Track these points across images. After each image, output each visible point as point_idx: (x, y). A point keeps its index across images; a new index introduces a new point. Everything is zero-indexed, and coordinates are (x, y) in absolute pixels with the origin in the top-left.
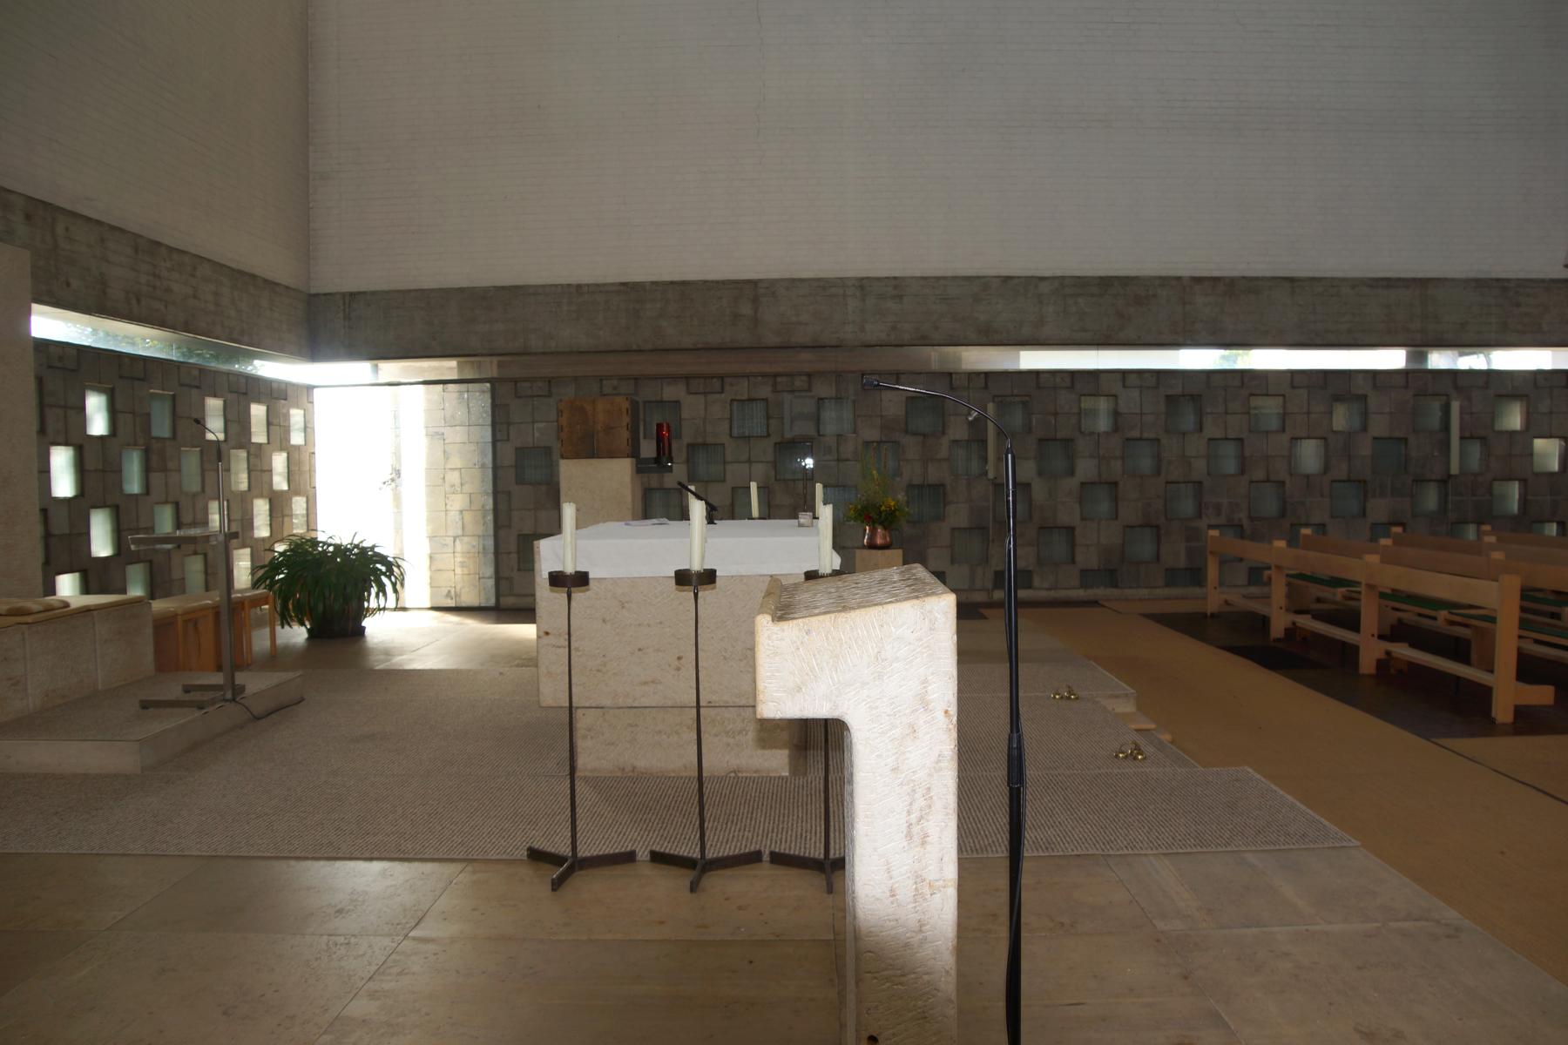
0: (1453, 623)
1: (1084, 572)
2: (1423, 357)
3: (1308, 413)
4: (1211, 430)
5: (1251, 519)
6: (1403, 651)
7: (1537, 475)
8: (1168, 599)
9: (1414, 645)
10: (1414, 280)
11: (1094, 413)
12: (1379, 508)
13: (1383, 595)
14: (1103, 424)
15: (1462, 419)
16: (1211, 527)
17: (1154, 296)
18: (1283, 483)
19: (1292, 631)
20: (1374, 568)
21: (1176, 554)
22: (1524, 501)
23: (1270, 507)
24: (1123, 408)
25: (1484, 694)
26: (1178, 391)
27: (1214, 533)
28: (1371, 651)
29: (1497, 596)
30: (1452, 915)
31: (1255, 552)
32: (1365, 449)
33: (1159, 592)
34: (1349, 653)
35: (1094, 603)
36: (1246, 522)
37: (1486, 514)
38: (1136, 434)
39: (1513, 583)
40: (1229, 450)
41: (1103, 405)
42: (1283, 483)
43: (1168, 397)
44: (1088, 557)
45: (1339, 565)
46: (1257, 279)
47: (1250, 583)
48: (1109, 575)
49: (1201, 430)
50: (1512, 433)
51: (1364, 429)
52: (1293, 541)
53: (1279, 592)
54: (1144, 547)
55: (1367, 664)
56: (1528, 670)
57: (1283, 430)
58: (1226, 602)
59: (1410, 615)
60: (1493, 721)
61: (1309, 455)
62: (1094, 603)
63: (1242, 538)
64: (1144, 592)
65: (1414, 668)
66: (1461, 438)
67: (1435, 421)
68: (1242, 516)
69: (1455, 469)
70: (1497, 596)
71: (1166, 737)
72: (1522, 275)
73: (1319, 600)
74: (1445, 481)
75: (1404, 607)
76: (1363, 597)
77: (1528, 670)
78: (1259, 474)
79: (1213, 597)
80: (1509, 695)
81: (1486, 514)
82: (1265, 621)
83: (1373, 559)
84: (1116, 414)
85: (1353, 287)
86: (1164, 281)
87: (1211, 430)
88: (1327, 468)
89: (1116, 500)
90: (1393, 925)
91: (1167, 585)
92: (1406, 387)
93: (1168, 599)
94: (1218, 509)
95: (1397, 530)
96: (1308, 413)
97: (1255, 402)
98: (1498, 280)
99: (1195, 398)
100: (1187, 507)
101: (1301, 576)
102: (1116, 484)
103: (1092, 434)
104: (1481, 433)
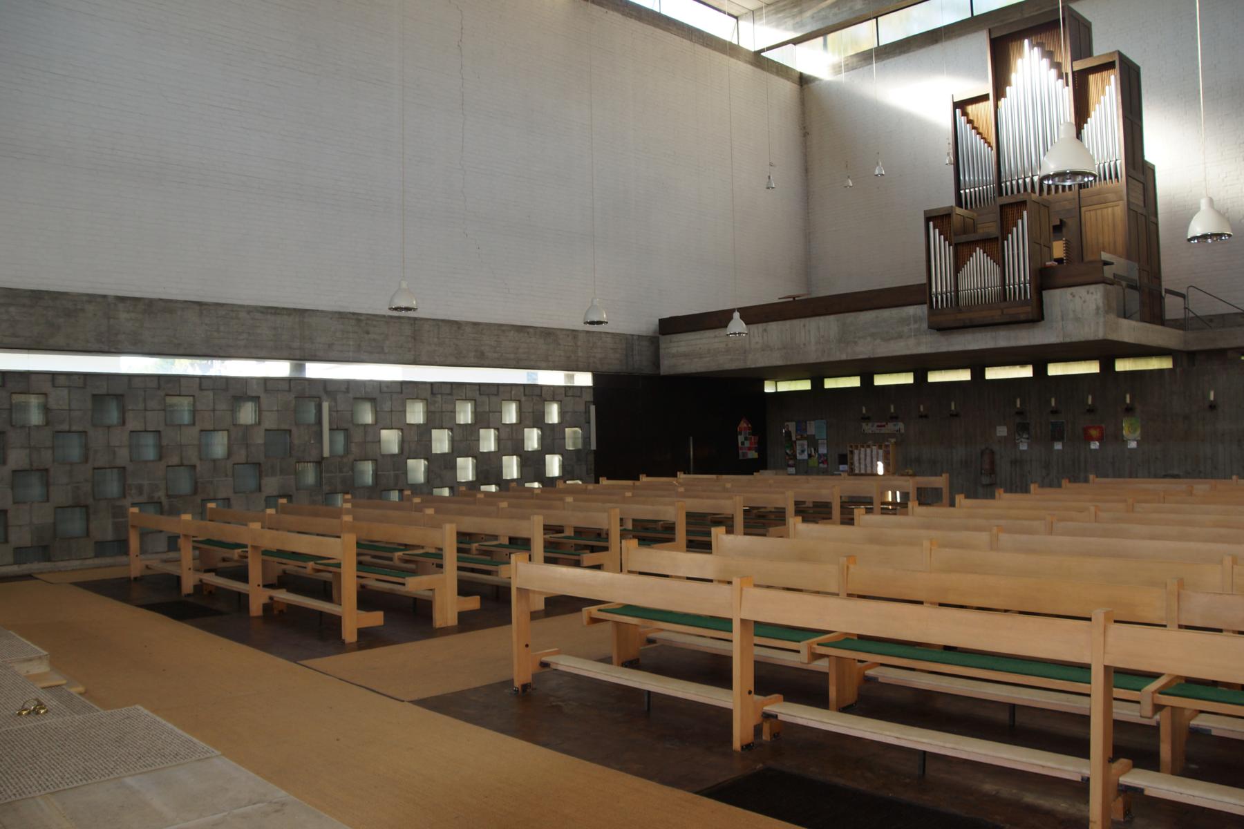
0: (319, 571)
1: (18, 550)
2: (301, 368)
3: (214, 410)
4: (133, 424)
5: (168, 496)
6: (283, 596)
7: (383, 456)
8: (100, 567)
9: (290, 590)
10: (295, 310)
11: (25, 407)
12: (272, 484)
13: (266, 553)
14: (35, 418)
15: (330, 415)
16: (134, 505)
17: (83, 310)
18: (194, 467)
19: (200, 587)
20: (256, 533)
21: (104, 528)
22: (376, 475)
23: (184, 486)
24: (52, 404)
25: (334, 623)
26: (103, 391)
27: (135, 510)
28: (258, 598)
29: (341, 549)
30: (281, 794)
31: (169, 525)
32: (259, 439)
33: (89, 562)
34: (241, 600)
35: (29, 577)
36: (164, 500)
37: (350, 486)
38: (65, 427)
39: (350, 539)
40: (149, 440)
41: (34, 401)
42: (194, 467)
43: (94, 396)
44: (21, 536)
45: (230, 532)
46: (171, 301)
47: (169, 550)
48: (44, 549)
49: (124, 423)
50: (366, 426)
51: (259, 423)
52: (202, 514)
53: (187, 555)
54: (75, 525)
55: (256, 608)
56: (367, 600)
57: (194, 424)
58: (147, 567)
59: (291, 566)
60: (343, 642)
61: (219, 445)
62: (29, 577)
63: (162, 513)
64: (76, 564)
65: (292, 607)
66: (331, 430)
67: (311, 417)
68: (161, 494)
69: (326, 453)
70: (341, 549)
71: (76, 690)
72: (370, 312)
73: (224, 560)
74: (319, 462)
75: (284, 561)
76: (249, 554)
77: (367, 600)
78: (175, 460)
79: (136, 564)
80: (353, 619)
81: (350, 486)
82: (178, 579)
83: (256, 526)
84: (46, 409)
85: (249, 312)
86: (92, 298)
87: (133, 424)
88: (230, 454)
89: (47, 485)
90: (236, 811)
91: (96, 556)
92: (290, 390)
93: (100, 567)
94: (140, 489)
95: (284, 501)
96: (214, 410)
97: (169, 400)
98: (354, 314)
99: (119, 397)
100: (113, 488)
101: (209, 542)
102: (47, 470)
103: (23, 427)
104: (346, 426)
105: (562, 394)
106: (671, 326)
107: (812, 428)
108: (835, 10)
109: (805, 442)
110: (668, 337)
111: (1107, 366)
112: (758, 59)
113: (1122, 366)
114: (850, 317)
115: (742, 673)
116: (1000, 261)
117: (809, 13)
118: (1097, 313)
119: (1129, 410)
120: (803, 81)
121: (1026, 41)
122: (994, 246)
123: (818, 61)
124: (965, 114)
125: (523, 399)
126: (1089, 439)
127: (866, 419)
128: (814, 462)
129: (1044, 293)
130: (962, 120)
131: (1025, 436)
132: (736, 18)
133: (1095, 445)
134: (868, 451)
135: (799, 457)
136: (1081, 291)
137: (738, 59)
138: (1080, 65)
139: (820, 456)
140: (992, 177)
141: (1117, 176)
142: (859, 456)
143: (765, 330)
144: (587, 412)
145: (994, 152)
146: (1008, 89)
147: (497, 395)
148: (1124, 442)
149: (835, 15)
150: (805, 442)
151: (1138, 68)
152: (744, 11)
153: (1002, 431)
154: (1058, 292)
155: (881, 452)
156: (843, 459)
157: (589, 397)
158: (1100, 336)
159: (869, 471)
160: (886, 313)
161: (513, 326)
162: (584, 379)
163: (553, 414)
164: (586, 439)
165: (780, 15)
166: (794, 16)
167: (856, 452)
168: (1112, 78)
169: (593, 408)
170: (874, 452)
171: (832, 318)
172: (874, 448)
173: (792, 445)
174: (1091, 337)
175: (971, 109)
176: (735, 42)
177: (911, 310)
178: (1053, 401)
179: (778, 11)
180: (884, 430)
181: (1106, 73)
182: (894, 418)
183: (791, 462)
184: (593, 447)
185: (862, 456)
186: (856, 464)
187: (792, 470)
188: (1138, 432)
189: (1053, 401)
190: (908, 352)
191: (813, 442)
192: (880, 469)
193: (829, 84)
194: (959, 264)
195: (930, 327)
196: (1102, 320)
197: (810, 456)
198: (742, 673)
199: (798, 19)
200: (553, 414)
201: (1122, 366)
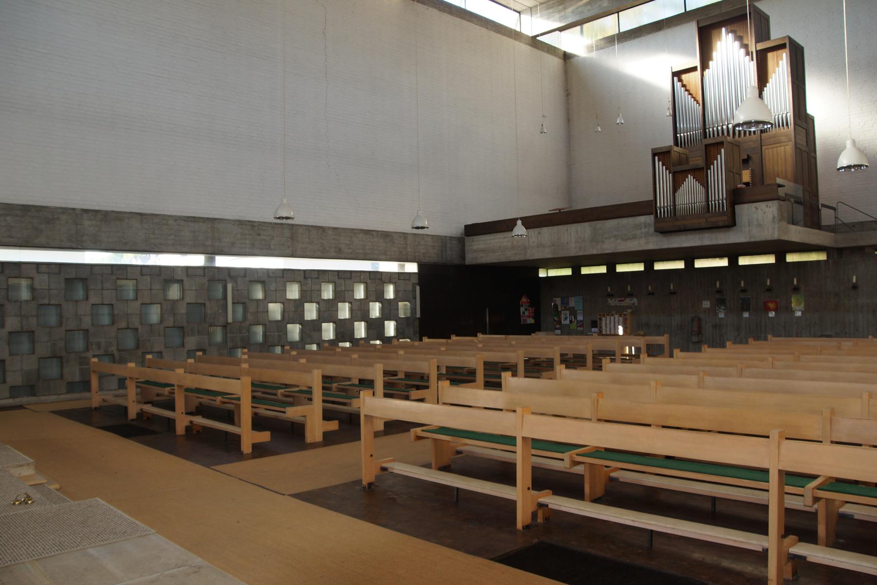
0: (225, 403)
1: (13, 388)
2: (212, 260)
3: (151, 289)
4: (93, 299)
5: (119, 350)
6: (199, 420)
7: (270, 322)
8: (70, 400)
9: (204, 416)
10: (208, 219)
11: (17, 287)
12: (191, 342)
13: (188, 390)
14: (25, 295)
15: (233, 293)
16: (94, 356)
17: (58, 219)
18: (137, 329)
19: (141, 414)
20: (181, 376)
21: (73, 373)
22: (265, 335)
23: (130, 343)
24: (37, 285)
25: (236, 440)
26: (73, 276)
27: (95, 360)
28: (182, 422)
29: (240, 388)
30: (198, 561)
31: (119, 370)
32: (182, 309)
33: (63, 397)
34: (170, 424)
35: (20, 407)
36: (116, 353)
37: (247, 343)
38: (46, 301)
39: (247, 380)
40: (105, 310)
41: (24, 283)
42: (137, 329)
43: (66, 279)
44: (15, 378)
45: (162, 375)
46: (121, 212)
47: (119, 388)
48: (31, 388)
49: (87, 299)
50: (258, 300)
51: (183, 299)
52: (142, 363)
53: (132, 391)
54: (53, 370)
55: (180, 429)
56: (258, 423)
57: (137, 299)
58: (104, 400)
59: (205, 399)
60: (242, 453)
61: (154, 314)
62: (20, 407)
63: (114, 362)
64: (53, 398)
65: (206, 429)
66: (233, 303)
67: (219, 294)
68: (113, 349)
69: (230, 320)
70: (240, 388)
71: (54, 487)
72: (261, 220)
73: (158, 395)
74: (225, 326)
75: (200, 396)
76: (176, 391)
77: (258, 423)
78: (123, 325)
79: (96, 398)
80: (249, 437)
81: (247, 343)
82: (126, 409)
83: (180, 371)
84: (32, 289)
85: (175, 220)
86: (65, 210)
87: (93, 299)
88: (162, 320)
89: (33, 342)
90: (166, 572)
91: (68, 393)
92: (204, 276)
93: (70, 400)
94: (99, 345)
95: (200, 353)
96: (151, 289)
97: (119, 282)
98: (249, 221)
99: (84, 280)
100: (80, 345)
101: (147, 382)
102: (33, 332)
103: (16, 301)
104: (244, 300)
105: (396, 278)
106: (473, 230)
107: (572, 302)
108: (589, 7)
109: (568, 312)
110: (471, 238)
111: (780, 258)
112: (534, 42)
113: (791, 258)
114: (599, 224)
115: (523, 475)
116: (705, 184)
117: (570, 10)
118: (774, 221)
119: (796, 289)
120: (566, 57)
121: (723, 29)
122: (701, 173)
123: (577, 43)
124: (680, 80)
125: (369, 281)
126: (768, 310)
127: (611, 296)
128: (574, 326)
129: (736, 207)
130: (678, 85)
131: (723, 308)
132: (519, 12)
133: (772, 314)
134: (612, 318)
135: (563, 322)
136: (762, 205)
137: (521, 41)
138: (761, 46)
139: (578, 322)
140: (699, 125)
141: (787, 124)
142: (606, 322)
143: (539, 233)
144: (414, 291)
145: (701, 107)
146: (711, 63)
147: (350, 278)
148: (792, 312)
149: (589, 10)
150: (568, 312)
151: (803, 48)
152: (525, 8)
153: (706, 304)
154: (746, 206)
155: (621, 319)
156: (594, 324)
157: (415, 280)
158: (776, 237)
159: (613, 333)
160: (625, 221)
161: (362, 230)
162: (412, 268)
163: (390, 292)
164: (413, 310)
165: (550, 11)
166: (560, 11)
167: (604, 319)
168: (784, 55)
169: (418, 288)
170: (616, 319)
171: (586, 224)
172: (616, 316)
173: (559, 314)
174: (769, 238)
175: (684, 77)
176: (518, 30)
177: (642, 219)
178: (742, 283)
179: (548, 8)
180: (623, 304)
181: (779, 52)
182: (630, 295)
183: (558, 326)
184: (418, 315)
185: (608, 322)
186: (604, 327)
187: (558, 332)
188: (802, 305)
189: (742, 283)
190: (640, 249)
191: (573, 312)
192: (621, 331)
193: (584, 59)
194: (676, 186)
195: (656, 231)
196: (777, 226)
197: (571, 322)
198: (523, 475)
199: (562, 14)
200: (390, 292)
201: (791, 258)
